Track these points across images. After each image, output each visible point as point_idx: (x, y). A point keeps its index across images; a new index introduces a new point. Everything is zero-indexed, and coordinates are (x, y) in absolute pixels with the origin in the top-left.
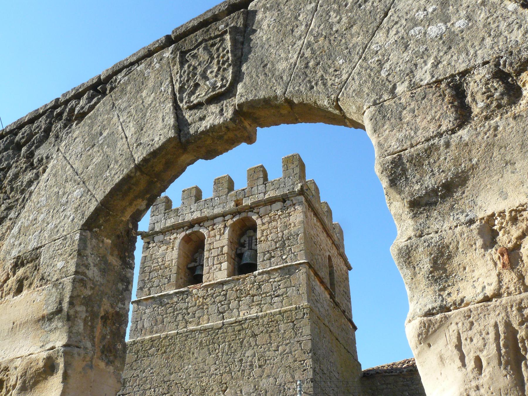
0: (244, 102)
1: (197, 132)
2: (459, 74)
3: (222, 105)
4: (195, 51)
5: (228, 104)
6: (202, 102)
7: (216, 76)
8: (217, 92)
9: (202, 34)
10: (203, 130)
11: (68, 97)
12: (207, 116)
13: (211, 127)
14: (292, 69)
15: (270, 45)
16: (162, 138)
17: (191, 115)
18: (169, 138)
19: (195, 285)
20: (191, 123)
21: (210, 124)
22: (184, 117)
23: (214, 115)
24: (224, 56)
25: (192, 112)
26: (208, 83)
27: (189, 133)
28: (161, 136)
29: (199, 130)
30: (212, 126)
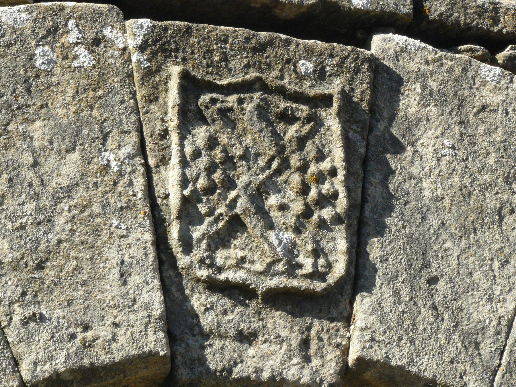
0: (378, 361)
1: (230, 372)
2: (497, 367)
3: (309, 329)
4: (232, 100)
5: (325, 337)
6: (254, 291)
7: (298, 230)
8: (295, 283)
9: (244, 49)
10: (248, 377)
11: (354, 262)
12: (261, 339)
13: (272, 378)
14: (503, 335)
15: (443, 224)
16: (122, 340)
17: (212, 308)
18: (150, 352)
19: (12, 7)
20: (211, 332)
21: (273, 370)
22: (186, 299)
23: (285, 347)
24: (320, 178)
25: (214, 298)
26: (272, 235)
27: (202, 361)
28: (120, 332)
29: (236, 370)
30: (278, 379)
